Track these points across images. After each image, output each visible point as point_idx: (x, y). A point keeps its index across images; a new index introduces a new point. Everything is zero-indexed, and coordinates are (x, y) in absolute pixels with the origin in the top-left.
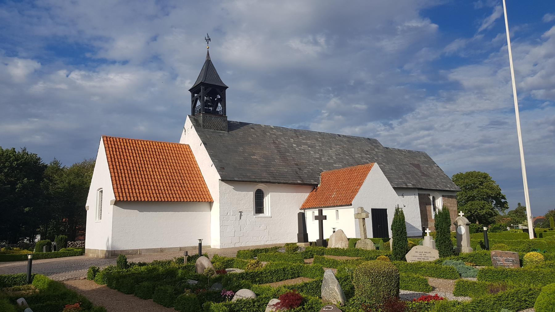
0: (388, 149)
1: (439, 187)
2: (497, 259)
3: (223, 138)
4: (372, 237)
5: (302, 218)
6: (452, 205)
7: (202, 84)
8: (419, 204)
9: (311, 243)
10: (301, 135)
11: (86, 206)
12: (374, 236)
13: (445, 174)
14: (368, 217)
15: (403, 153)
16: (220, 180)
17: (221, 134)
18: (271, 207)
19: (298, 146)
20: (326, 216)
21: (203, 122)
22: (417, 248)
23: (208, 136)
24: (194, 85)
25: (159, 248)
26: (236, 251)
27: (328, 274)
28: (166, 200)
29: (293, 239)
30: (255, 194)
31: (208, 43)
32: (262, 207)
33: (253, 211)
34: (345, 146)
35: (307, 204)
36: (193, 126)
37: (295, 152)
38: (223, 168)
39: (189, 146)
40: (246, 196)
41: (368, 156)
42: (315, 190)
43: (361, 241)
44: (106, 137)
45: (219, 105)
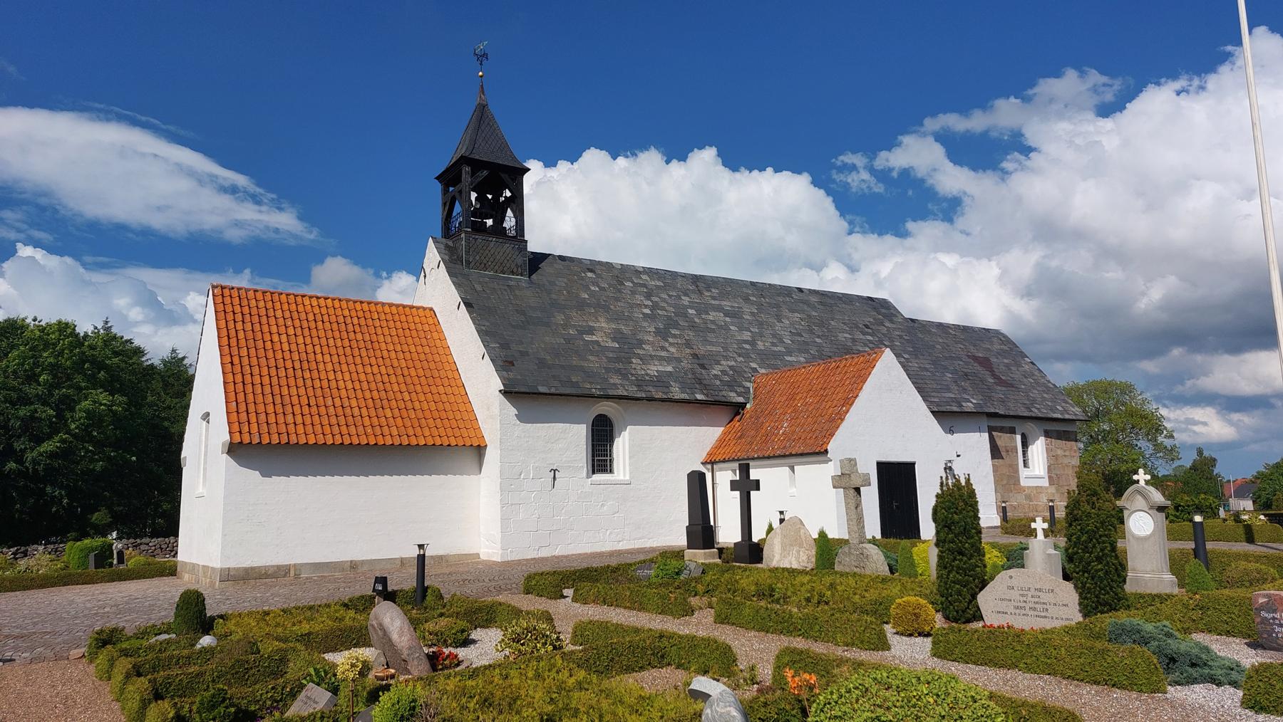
1: (1036, 411)
2: (1274, 618)
4: (879, 536)
5: (697, 483)
6: (1067, 453)
7: (463, 160)
8: (991, 452)
9: (721, 550)
10: (708, 288)
11: (182, 456)
12: (885, 533)
13: (1049, 382)
14: (870, 485)
15: (951, 331)
16: (500, 391)
17: (512, 283)
18: (630, 458)
19: (699, 313)
20: (758, 482)
21: (467, 252)
22: (1011, 577)
23: (479, 288)
25: (347, 561)
27: (717, 712)
28: (256, 440)
30: (593, 426)
31: (481, 64)
33: (585, 469)
34: (814, 313)
35: (719, 452)
36: (441, 262)
37: (693, 326)
39: (434, 311)
40: (567, 431)
41: (870, 338)
42: (738, 418)
43: (850, 548)
44: (221, 287)
45: (509, 213)
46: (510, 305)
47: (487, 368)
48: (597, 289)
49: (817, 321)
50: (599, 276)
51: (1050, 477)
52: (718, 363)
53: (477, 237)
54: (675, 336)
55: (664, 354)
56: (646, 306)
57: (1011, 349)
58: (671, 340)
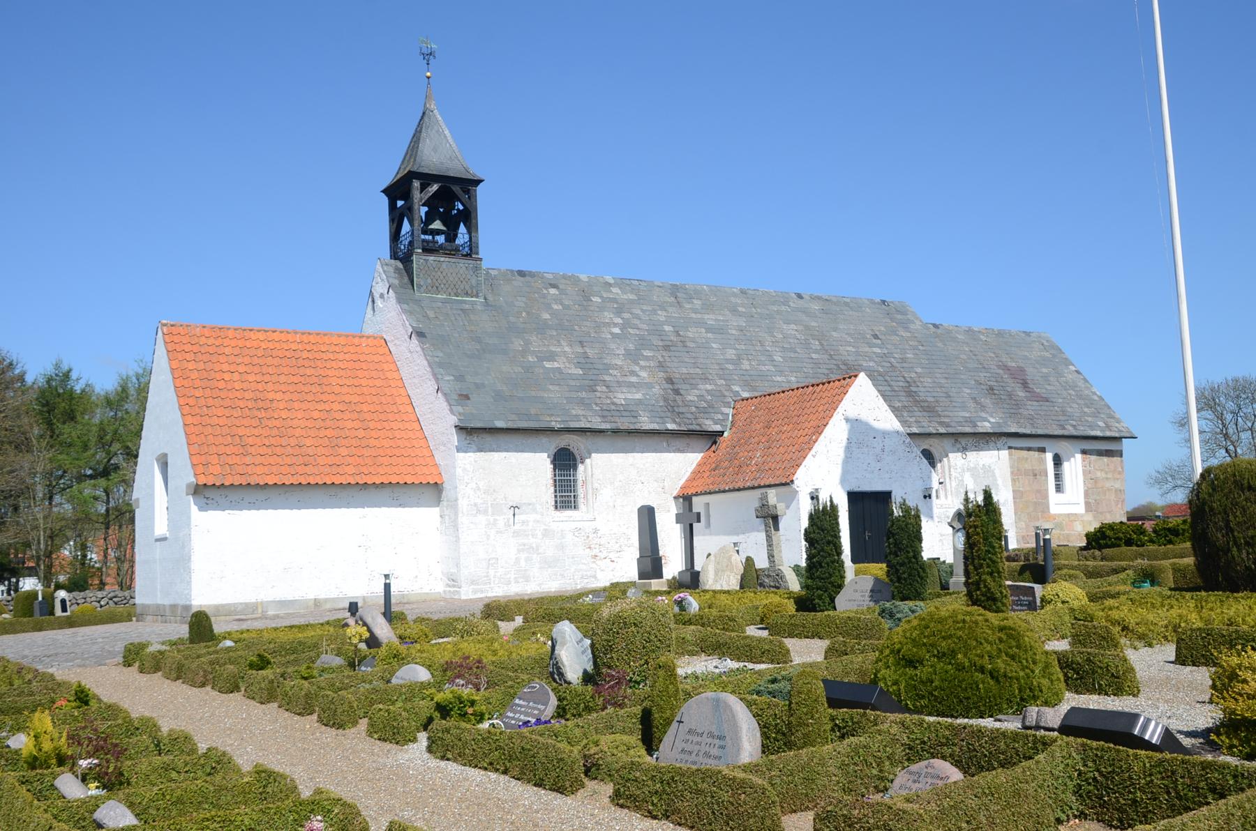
0: (938, 328)
1: (1071, 428)
3: (472, 317)
6: (1110, 476)
15: (982, 337)
23: (431, 314)
24: (396, 176)
26: (481, 606)
29: (627, 570)
32: (572, 494)
34: (814, 324)
38: (467, 397)
41: (877, 350)
46: (465, 332)
47: (441, 403)
48: (561, 307)
49: (816, 333)
50: (562, 292)
51: (1087, 504)
52: (694, 386)
53: (427, 258)
54: (647, 358)
55: (634, 379)
56: (615, 325)
57: (1054, 356)
58: (642, 363)
